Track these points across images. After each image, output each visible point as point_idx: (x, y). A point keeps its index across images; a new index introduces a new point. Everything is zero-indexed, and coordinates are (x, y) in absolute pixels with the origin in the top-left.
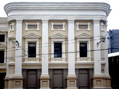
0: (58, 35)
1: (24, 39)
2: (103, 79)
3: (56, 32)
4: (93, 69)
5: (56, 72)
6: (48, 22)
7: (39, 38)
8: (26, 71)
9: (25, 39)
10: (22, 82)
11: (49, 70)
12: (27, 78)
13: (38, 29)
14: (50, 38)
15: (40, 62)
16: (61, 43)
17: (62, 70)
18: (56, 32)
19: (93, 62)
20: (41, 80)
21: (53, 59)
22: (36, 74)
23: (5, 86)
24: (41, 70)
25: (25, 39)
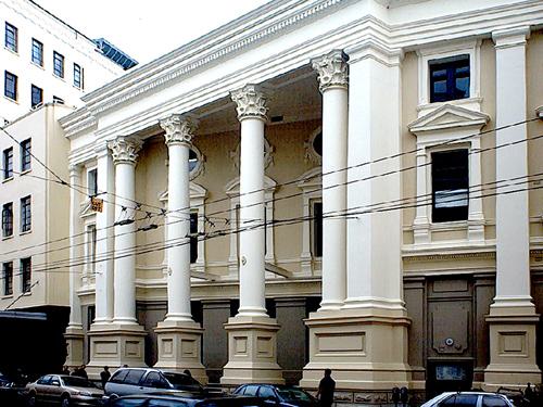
2: (72, 338)
4: (491, 279)
5: (438, 287)
6: (397, 61)
7: (483, 127)
8: (422, 285)
9: (414, 135)
11: (405, 282)
12: (428, 321)
17: (469, 279)
19: (490, 243)
20: (492, 328)
21: (424, 233)
22: (472, 300)
23: (534, 350)
24: (494, 278)
25: (414, 135)
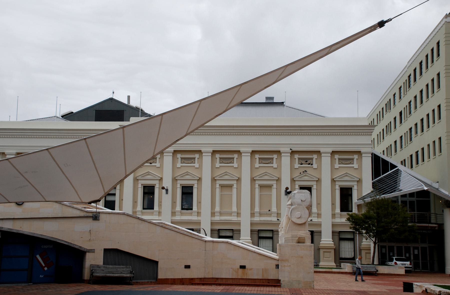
0: (187, 174)
1: (175, 180)
3: (262, 171)
9: (295, 181)
10: (333, 251)
13: (275, 165)
14: (333, 181)
15: (239, 219)
16: (352, 188)
18: (262, 171)
